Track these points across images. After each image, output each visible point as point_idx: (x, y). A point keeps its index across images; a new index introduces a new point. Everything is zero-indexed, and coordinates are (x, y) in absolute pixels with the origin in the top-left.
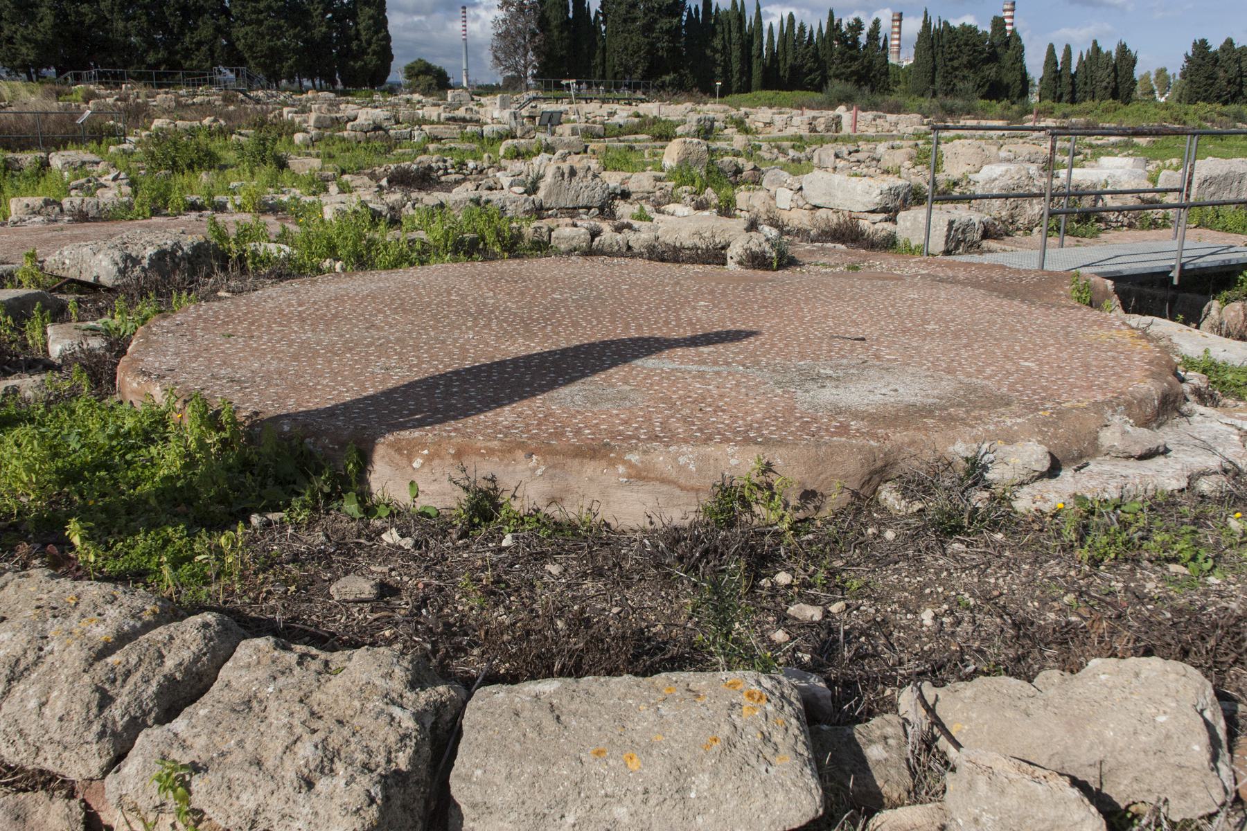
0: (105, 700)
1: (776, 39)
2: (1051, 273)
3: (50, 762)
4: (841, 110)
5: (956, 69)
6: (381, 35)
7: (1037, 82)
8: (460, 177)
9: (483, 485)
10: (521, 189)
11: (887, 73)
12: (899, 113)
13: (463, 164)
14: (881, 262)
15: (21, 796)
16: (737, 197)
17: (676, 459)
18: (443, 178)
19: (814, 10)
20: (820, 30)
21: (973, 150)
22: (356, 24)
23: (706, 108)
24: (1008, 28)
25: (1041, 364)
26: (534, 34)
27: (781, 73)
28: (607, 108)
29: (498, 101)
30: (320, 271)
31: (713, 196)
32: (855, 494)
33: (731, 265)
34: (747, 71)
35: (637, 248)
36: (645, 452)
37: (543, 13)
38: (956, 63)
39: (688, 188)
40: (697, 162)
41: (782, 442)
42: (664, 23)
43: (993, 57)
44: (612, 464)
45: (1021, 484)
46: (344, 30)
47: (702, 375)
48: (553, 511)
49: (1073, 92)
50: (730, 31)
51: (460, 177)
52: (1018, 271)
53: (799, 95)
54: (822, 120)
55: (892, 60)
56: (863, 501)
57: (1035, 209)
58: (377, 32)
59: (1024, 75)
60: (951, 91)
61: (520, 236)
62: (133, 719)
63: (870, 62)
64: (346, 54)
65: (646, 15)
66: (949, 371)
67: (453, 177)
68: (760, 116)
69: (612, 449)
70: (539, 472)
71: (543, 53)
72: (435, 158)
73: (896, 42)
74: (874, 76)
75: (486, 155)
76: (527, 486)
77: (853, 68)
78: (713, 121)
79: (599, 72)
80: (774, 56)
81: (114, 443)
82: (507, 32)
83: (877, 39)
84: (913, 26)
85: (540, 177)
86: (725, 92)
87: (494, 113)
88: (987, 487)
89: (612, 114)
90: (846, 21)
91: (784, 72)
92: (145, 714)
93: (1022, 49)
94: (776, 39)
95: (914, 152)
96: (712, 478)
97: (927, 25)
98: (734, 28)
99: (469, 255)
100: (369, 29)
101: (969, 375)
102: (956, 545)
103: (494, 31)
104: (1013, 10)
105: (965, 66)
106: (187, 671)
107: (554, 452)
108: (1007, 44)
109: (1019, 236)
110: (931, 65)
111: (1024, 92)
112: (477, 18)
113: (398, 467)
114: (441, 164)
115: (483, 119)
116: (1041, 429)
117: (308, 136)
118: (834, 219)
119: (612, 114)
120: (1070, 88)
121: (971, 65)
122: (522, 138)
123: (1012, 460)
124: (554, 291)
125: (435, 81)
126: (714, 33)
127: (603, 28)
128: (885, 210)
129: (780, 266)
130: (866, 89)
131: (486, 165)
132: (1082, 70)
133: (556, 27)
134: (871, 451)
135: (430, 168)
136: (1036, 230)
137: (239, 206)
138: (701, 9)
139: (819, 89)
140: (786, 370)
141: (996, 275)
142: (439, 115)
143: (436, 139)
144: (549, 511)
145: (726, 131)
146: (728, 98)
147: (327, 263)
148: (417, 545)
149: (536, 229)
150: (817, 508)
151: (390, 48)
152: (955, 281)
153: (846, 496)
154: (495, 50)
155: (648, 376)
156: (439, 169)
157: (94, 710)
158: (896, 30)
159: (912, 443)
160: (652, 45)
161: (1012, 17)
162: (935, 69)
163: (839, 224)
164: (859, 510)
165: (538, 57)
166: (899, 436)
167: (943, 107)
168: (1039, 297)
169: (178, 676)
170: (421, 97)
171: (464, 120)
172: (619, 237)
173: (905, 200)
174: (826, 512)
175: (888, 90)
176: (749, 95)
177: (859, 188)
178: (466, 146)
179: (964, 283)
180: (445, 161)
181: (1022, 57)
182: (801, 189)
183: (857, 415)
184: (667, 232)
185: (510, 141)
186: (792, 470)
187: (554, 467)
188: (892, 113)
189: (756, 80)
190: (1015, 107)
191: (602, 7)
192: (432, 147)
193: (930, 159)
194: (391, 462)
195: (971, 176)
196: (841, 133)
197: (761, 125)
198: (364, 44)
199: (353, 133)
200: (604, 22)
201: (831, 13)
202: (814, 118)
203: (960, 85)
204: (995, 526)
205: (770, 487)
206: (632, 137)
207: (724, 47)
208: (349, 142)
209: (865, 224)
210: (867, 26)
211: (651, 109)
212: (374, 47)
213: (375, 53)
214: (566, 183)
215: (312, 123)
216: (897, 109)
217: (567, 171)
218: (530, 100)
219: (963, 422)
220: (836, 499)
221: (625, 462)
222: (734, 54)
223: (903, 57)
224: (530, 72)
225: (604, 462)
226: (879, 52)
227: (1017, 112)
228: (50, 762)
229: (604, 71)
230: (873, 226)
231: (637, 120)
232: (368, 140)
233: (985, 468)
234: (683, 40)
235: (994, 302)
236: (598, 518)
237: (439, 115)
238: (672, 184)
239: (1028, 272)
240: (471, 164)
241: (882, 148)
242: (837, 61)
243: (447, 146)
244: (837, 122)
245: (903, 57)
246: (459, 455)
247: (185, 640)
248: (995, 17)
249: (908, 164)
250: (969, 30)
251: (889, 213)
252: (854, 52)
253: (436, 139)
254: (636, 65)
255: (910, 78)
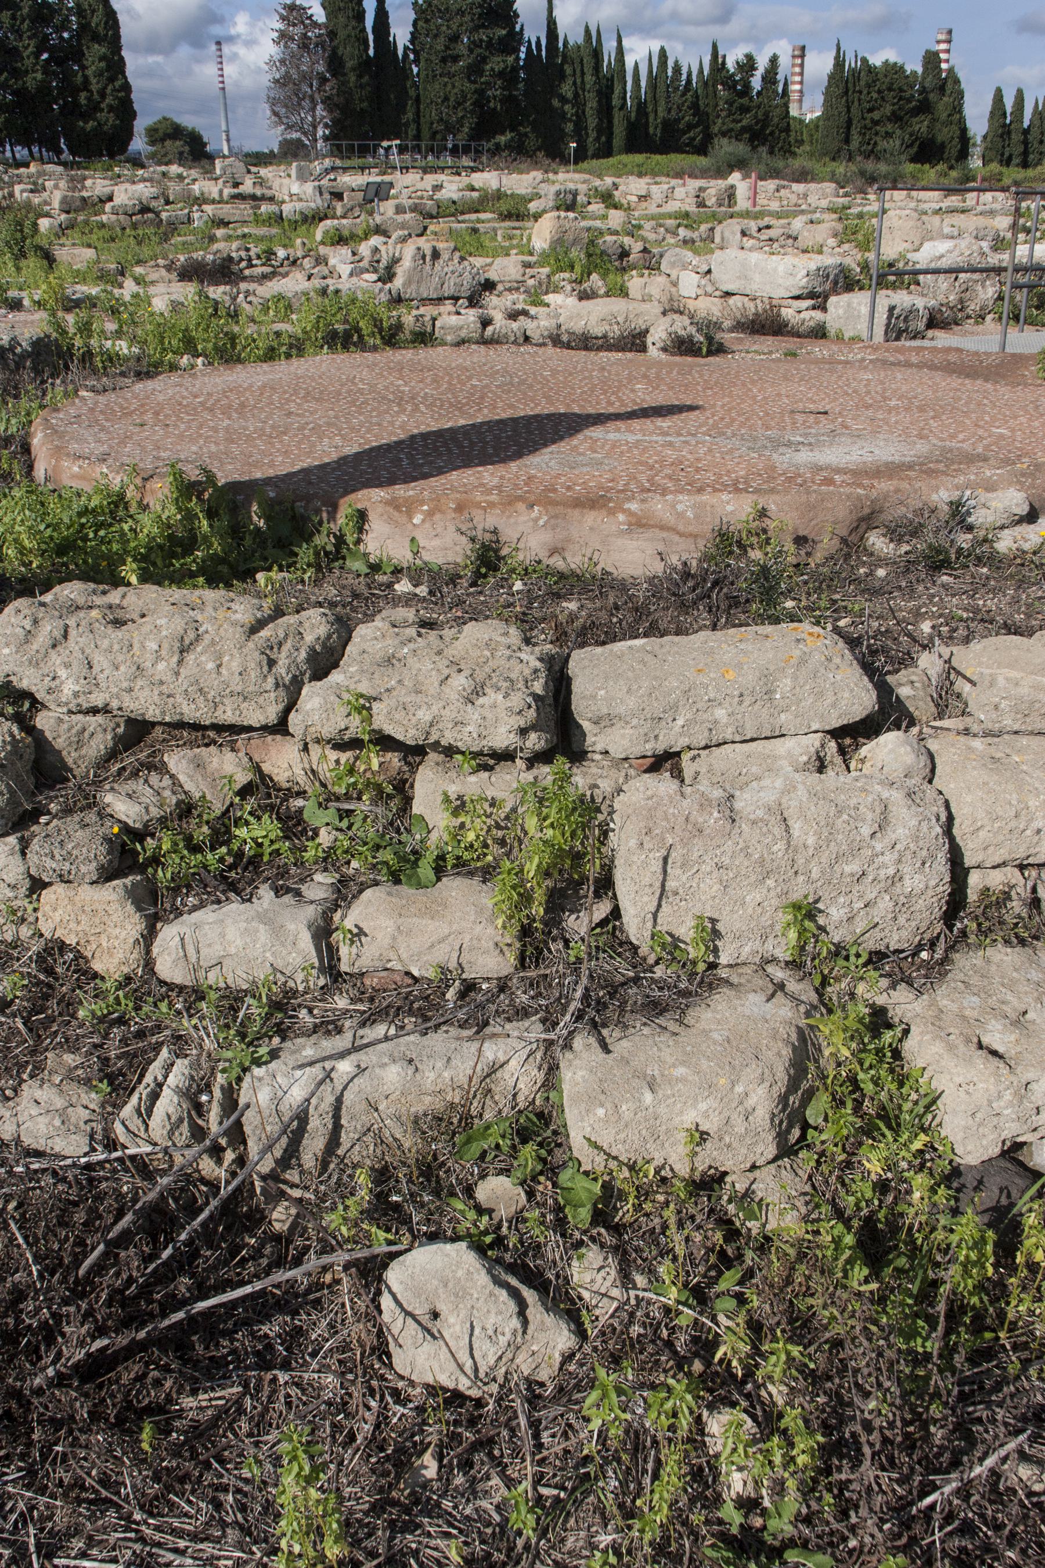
0: (272, 663)
1: (643, 84)
2: (1013, 355)
3: (229, 713)
4: (735, 178)
5: (876, 123)
6: (118, 84)
7: (979, 140)
8: (267, 270)
9: (488, 536)
10: (374, 277)
11: (787, 129)
12: (806, 181)
13: (270, 254)
14: (818, 349)
15: (197, 750)
16: (629, 284)
17: (673, 507)
18: (247, 272)
19: (688, 42)
20: (701, 71)
21: (911, 223)
22: (83, 68)
23: (561, 176)
24: (944, 66)
25: (1013, 431)
26: (323, 80)
27: (651, 130)
28: (431, 179)
29: (293, 172)
30: (173, 367)
31: (600, 283)
32: (844, 541)
33: (653, 352)
34: (606, 129)
35: (535, 336)
36: (643, 501)
37: (334, 50)
38: (876, 115)
39: (567, 275)
40: (575, 242)
41: (772, 491)
42: (496, 63)
43: (924, 107)
44: (612, 512)
45: (1002, 527)
46: (67, 78)
47: (671, 444)
48: (557, 563)
49: (1025, 153)
50: (583, 74)
51: (267, 270)
52: (977, 353)
53: (676, 159)
54: (712, 191)
55: (794, 112)
56: (852, 545)
57: (987, 292)
58: (112, 80)
59: (964, 130)
60: (872, 154)
61: (399, 327)
62: (295, 677)
63: (766, 114)
64: (72, 111)
65: (471, 51)
66: (921, 437)
67: (259, 270)
68: (632, 187)
69: (610, 500)
70: (541, 522)
71: (336, 105)
72: (235, 245)
73: (797, 87)
74: (772, 133)
75: (299, 241)
76: (528, 537)
77: (744, 123)
78: (575, 194)
79: (412, 131)
80: (641, 107)
81: (83, 520)
82: (287, 76)
83: (775, 82)
84: (820, 65)
85: (395, 261)
86: (581, 156)
87: (292, 188)
88: (970, 528)
89: (437, 188)
90: (732, 59)
91: (654, 129)
92: (303, 674)
93: (961, 95)
94: (643, 84)
95: (839, 227)
96: (707, 528)
97: (839, 63)
98: (588, 69)
99: (345, 347)
100: (101, 75)
101: (942, 440)
102: (945, 578)
103: (269, 77)
104: (949, 42)
105: (889, 119)
106: (324, 645)
107: (554, 503)
108: (942, 89)
109: (969, 325)
110: (844, 118)
111: (963, 154)
112: (235, 57)
113: (397, 525)
114: (243, 254)
115: (279, 197)
116: (1019, 480)
117: (56, 223)
118: (751, 307)
119: (437, 188)
120: (1021, 149)
121: (895, 117)
122: (344, 217)
123: (993, 504)
124: (470, 378)
125: (187, 148)
126: (562, 77)
127: (415, 70)
128: (811, 295)
129: (710, 353)
130: (763, 150)
131: (300, 254)
132: (1037, 123)
133: (353, 69)
134: (859, 498)
135: (230, 259)
136: (989, 318)
137: (39, 303)
138: (544, 42)
139: (702, 150)
140: (755, 439)
141: (953, 357)
142: (221, 192)
143: (224, 223)
144: (551, 561)
145: (590, 208)
146: (584, 165)
147: (185, 360)
148: (431, 593)
149: (417, 318)
150: (809, 554)
151: (130, 102)
152: (908, 365)
153: (836, 541)
154: (273, 102)
155: (614, 446)
156: (241, 260)
157: (265, 669)
158: (797, 70)
159: (897, 491)
160: (481, 92)
161: (948, 51)
162: (849, 123)
163: (756, 314)
164: (847, 557)
165: (330, 111)
166: (884, 486)
167: (862, 173)
168: (1004, 377)
169: (318, 648)
170: (180, 170)
171: (254, 197)
172: (515, 325)
173: (836, 283)
174: (819, 556)
175: (788, 152)
176: (611, 160)
177: (781, 268)
178: (263, 231)
179: (920, 366)
180: (248, 250)
181: (961, 105)
182: (709, 272)
183: (838, 471)
184: (571, 318)
185: (328, 222)
186: (785, 515)
187: (556, 517)
188: (798, 181)
189: (618, 141)
190: (954, 174)
191: (412, 42)
192: (220, 233)
193: (856, 232)
194: (390, 520)
195: (909, 256)
196: (737, 209)
197: (635, 199)
198: (96, 96)
199: (114, 217)
200: (416, 61)
201: (715, 47)
202: (702, 189)
203: (883, 144)
204: (979, 561)
205: (765, 531)
206: (474, 216)
207: (576, 95)
208: (111, 228)
209: (788, 313)
210: (762, 63)
211: (488, 179)
212: (109, 100)
213: (111, 109)
214: (428, 267)
215: (56, 204)
216: (802, 176)
217: (428, 253)
218: (327, 171)
219: (944, 473)
220: (827, 545)
221: (624, 511)
222: (589, 105)
223: (808, 107)
224: (320, 133)
225: (604, 512)
226: (778, 101)
227: (956, 180)
228: (229, 713)
229: (419, 130)
230: (793, 313)
231: (475, 194)
232: (134, 226)
233: (969, 513)
234: (521, 85)
235: (955, 382)
236: (599, 568)
237: (221, 192)
238: (545, 270)
239: (988, 354)
240: (281, 253)
241: (798, 224)
242: (723, 114)
243: (239, 232)
244: (731, 194)
245: (808, 107)
246: (460, 508)
247: (315, 625)
248: (927, 52)
249: (832, 242)
250: (894, 70)
251: (818, 299)
252: (744, 101)
253: (224, 223)
254: (460, 121)
255: (818, 135)
